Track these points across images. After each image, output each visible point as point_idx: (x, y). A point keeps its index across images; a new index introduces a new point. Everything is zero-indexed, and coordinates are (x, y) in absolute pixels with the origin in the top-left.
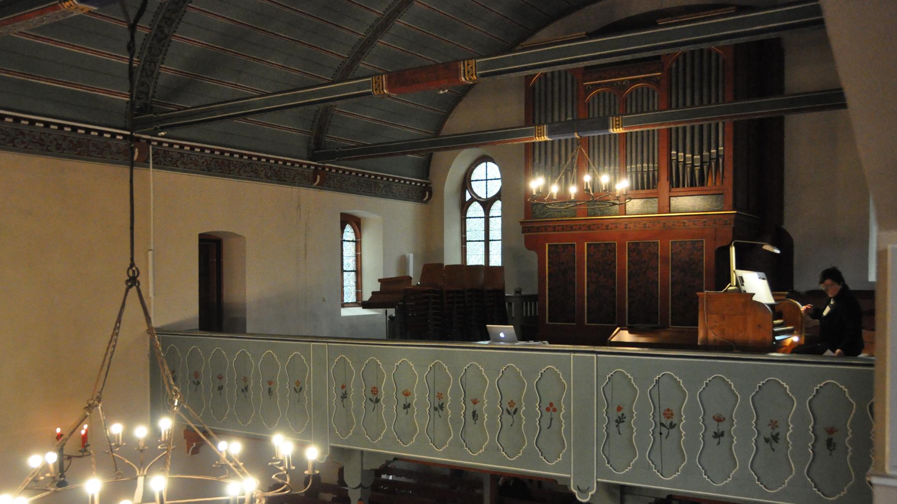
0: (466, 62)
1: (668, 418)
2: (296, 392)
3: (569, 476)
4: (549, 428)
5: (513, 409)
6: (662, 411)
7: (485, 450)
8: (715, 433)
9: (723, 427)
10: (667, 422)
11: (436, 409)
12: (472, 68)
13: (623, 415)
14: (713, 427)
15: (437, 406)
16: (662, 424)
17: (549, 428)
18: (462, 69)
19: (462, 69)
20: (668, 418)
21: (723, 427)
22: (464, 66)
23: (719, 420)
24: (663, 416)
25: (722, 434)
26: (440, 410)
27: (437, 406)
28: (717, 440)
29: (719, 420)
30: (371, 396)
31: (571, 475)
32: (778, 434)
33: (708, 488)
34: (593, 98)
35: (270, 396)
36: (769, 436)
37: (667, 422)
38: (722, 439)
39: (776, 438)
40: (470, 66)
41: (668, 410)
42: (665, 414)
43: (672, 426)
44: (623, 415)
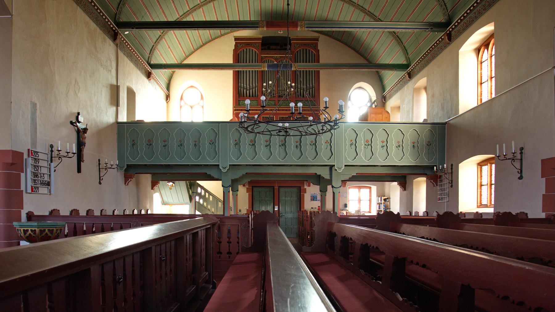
0: (301, 22)
1: (252, 142)
2: (311, 145)
3: (334, 164)
4: (326, 149)
5: (212, 143)
6: (365, 141)
7: (154, 158)
8: (266, 145)
9: (166, 143)
10: (149, 144)
11: (280, 146)
12: (303, 24)
13: (134, 142)
14: (163, 144)
15: (280, 144)
16: (365, 145)
17: (326, 149)
18: (299, 24)
19: (299, 24)
20: (367, 143)
21: (166, 143)
22: (300, 23)
23: (165, 141)
24: (365, 142)
25: (166, 146)
26: (282, 146)
27: (280, 144)
28: (266, 148)
29: (165, 141)
30: (147, 143)
31: (219, 163)
32: (182, 144)
33: (397, 163)
34: (241, 51)
35: (297, 149)
36: (179, 145)
37: (367, 144)
38: (166, 147)
39: (181, 145)
40: (302, 23)
41: (367, 140)
42: (366, 141)
43: (150, 145)
44: (237, 142)
